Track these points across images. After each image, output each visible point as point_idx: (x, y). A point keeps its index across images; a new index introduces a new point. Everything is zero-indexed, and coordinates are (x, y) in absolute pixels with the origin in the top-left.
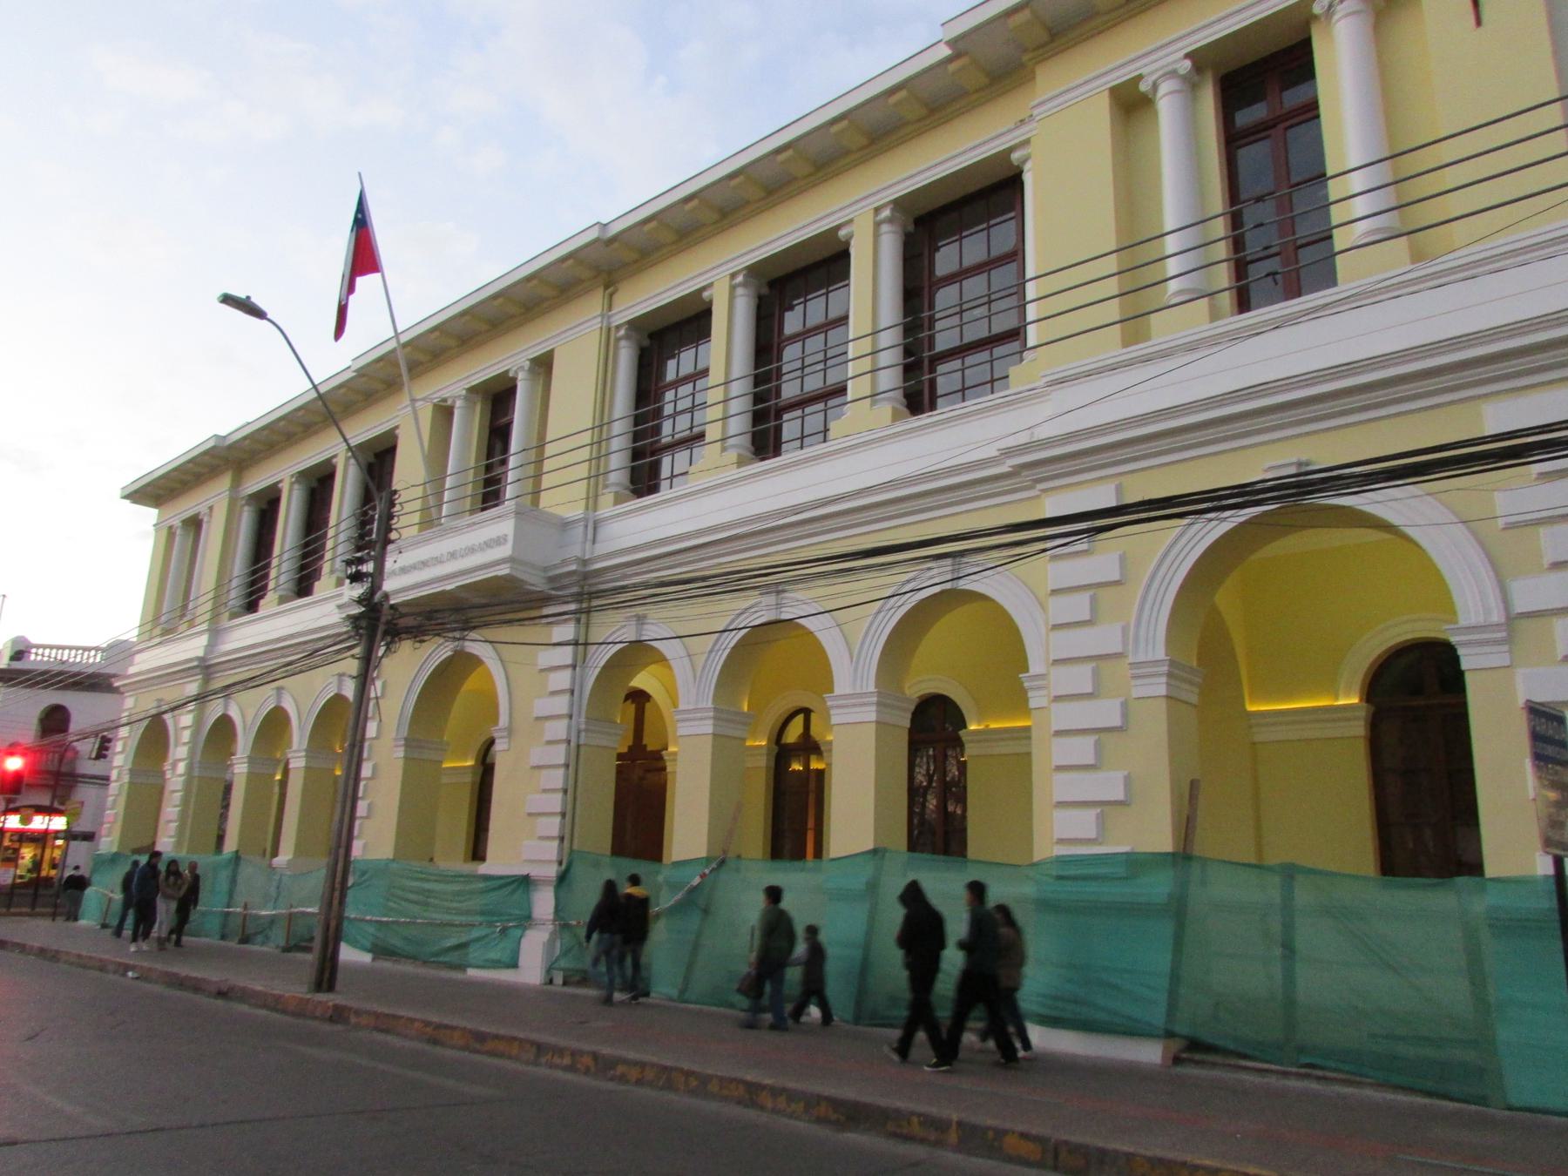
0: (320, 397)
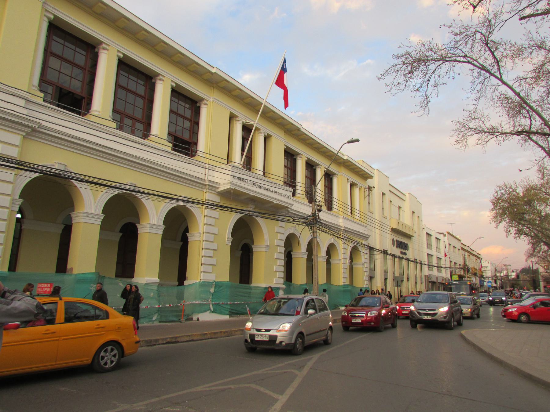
0: (337, 155)
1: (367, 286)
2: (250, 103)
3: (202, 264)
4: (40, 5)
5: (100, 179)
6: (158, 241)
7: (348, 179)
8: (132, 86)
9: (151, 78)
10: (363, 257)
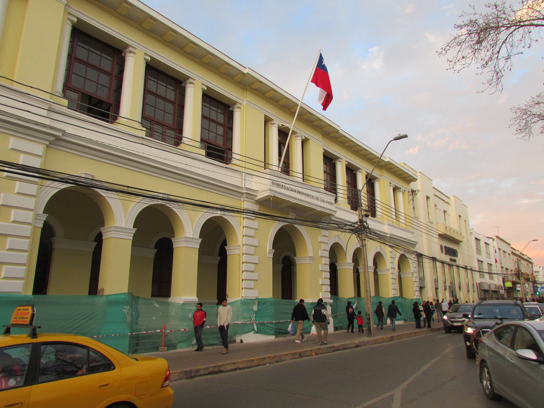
1: (418, 297)
2: (286, 106)
3: (243, 280)
4: (63, 6)
5: (128, 187)
6: (195, 256)
7: (390, 183)
9: (181, 82)
10: (412, 264)
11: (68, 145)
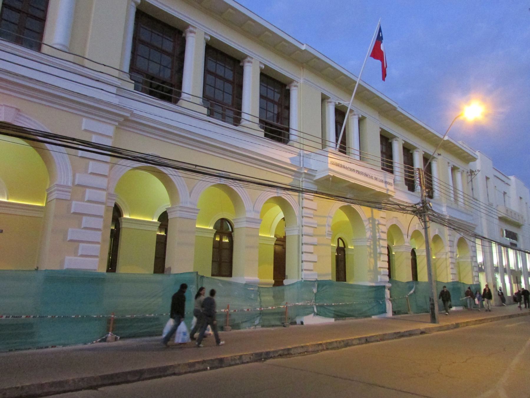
2: (344, 83)
5: (196, 166)
7: (448, 163)
8: (220, 71)
11: (135, 125)
